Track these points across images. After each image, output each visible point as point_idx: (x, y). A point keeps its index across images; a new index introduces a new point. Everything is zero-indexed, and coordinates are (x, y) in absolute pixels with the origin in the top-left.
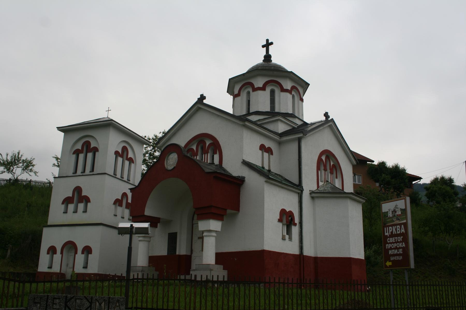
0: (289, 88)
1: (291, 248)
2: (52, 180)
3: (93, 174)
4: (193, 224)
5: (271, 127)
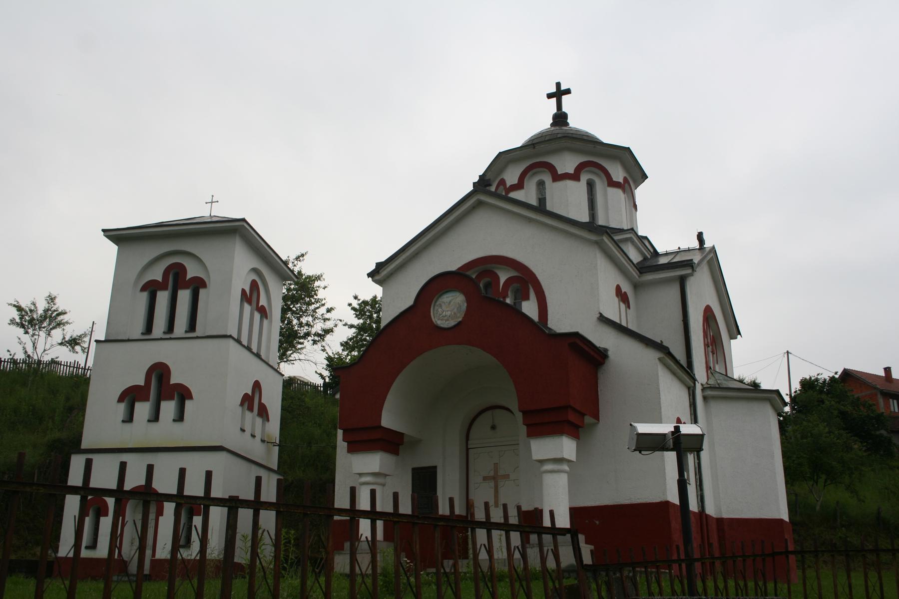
0: (571, 170)
3: (171, 339)
4: (468, 449)
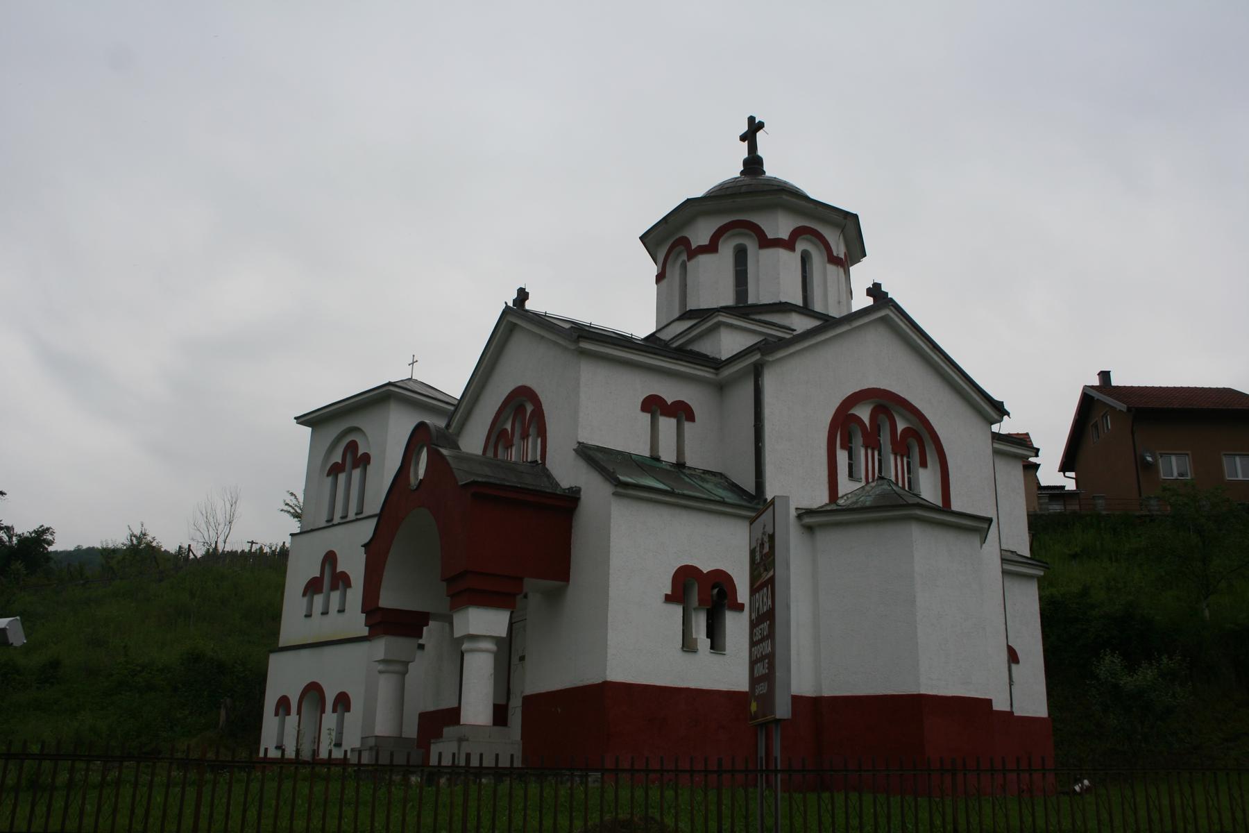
0: (784, 235)
1: (726, 671)
2: (288, 542)
5: (705, 347)
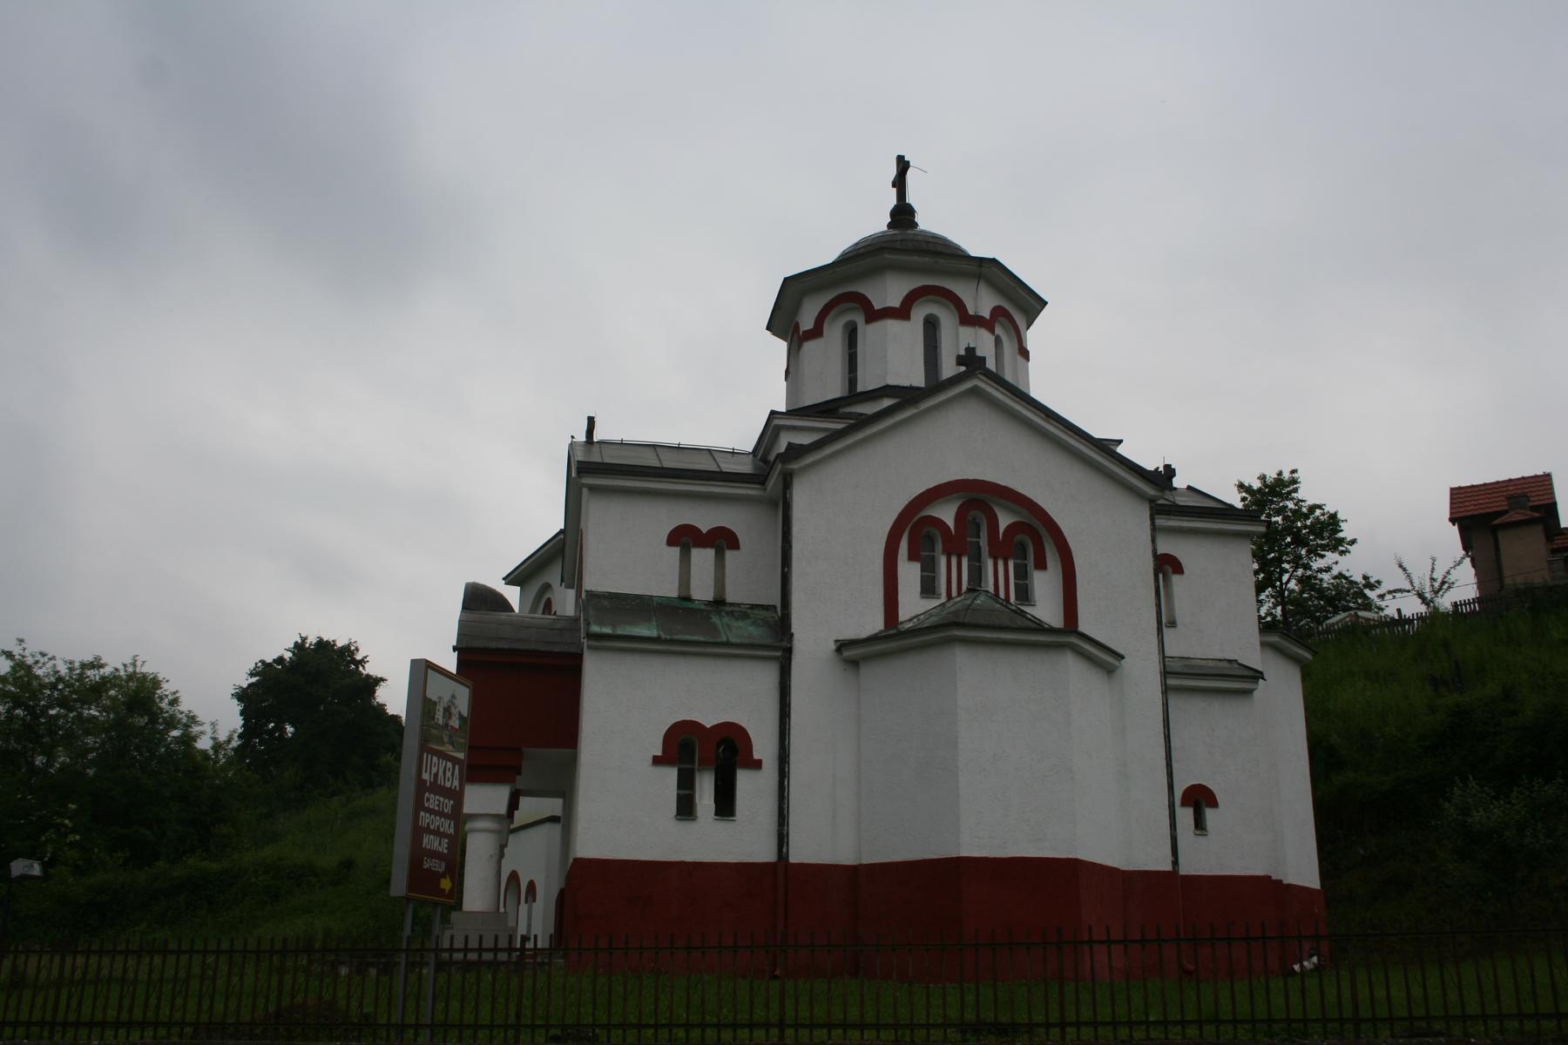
1: (742, 840)
